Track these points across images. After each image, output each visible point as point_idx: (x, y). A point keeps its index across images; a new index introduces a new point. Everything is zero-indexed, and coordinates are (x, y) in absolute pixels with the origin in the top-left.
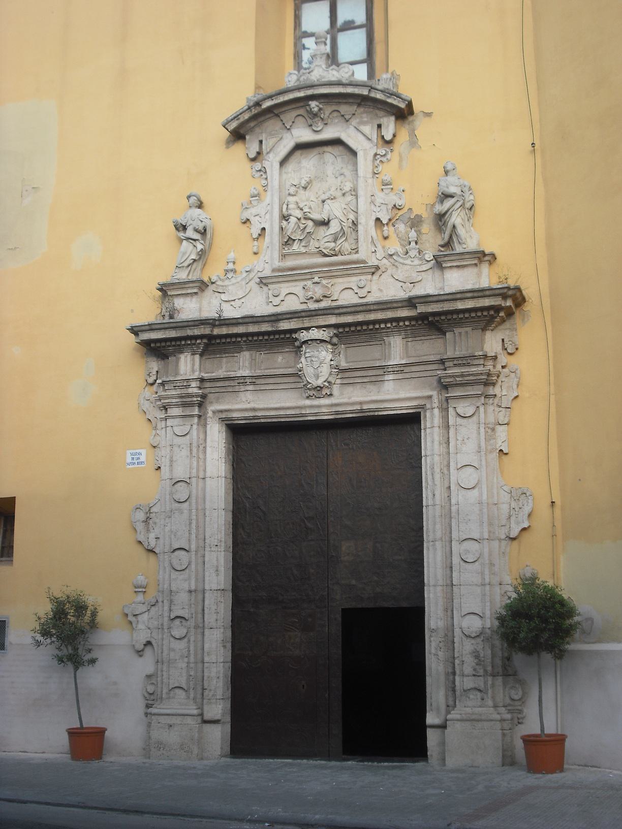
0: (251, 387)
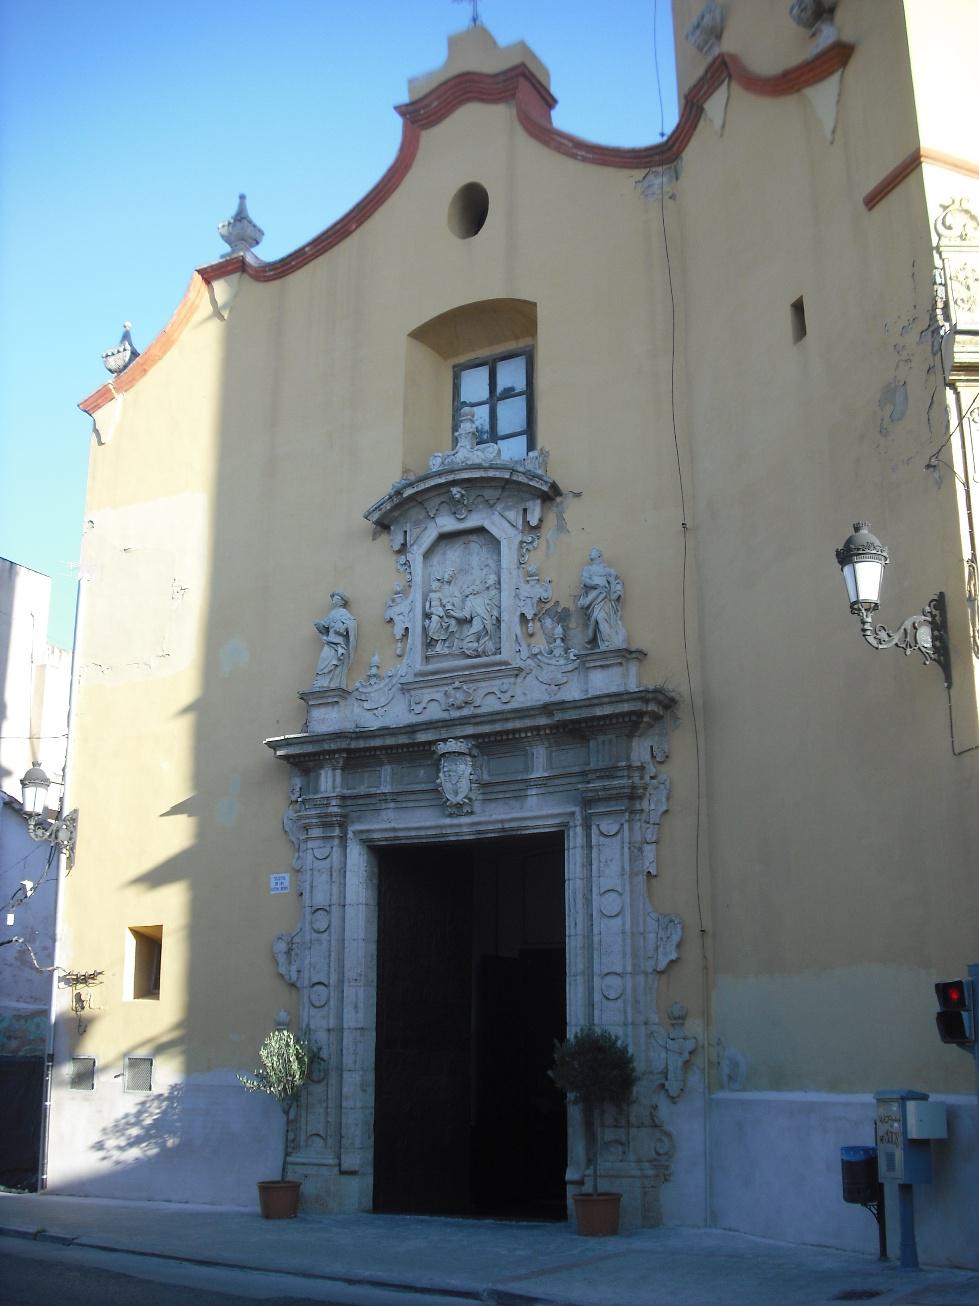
0: (392, 805)
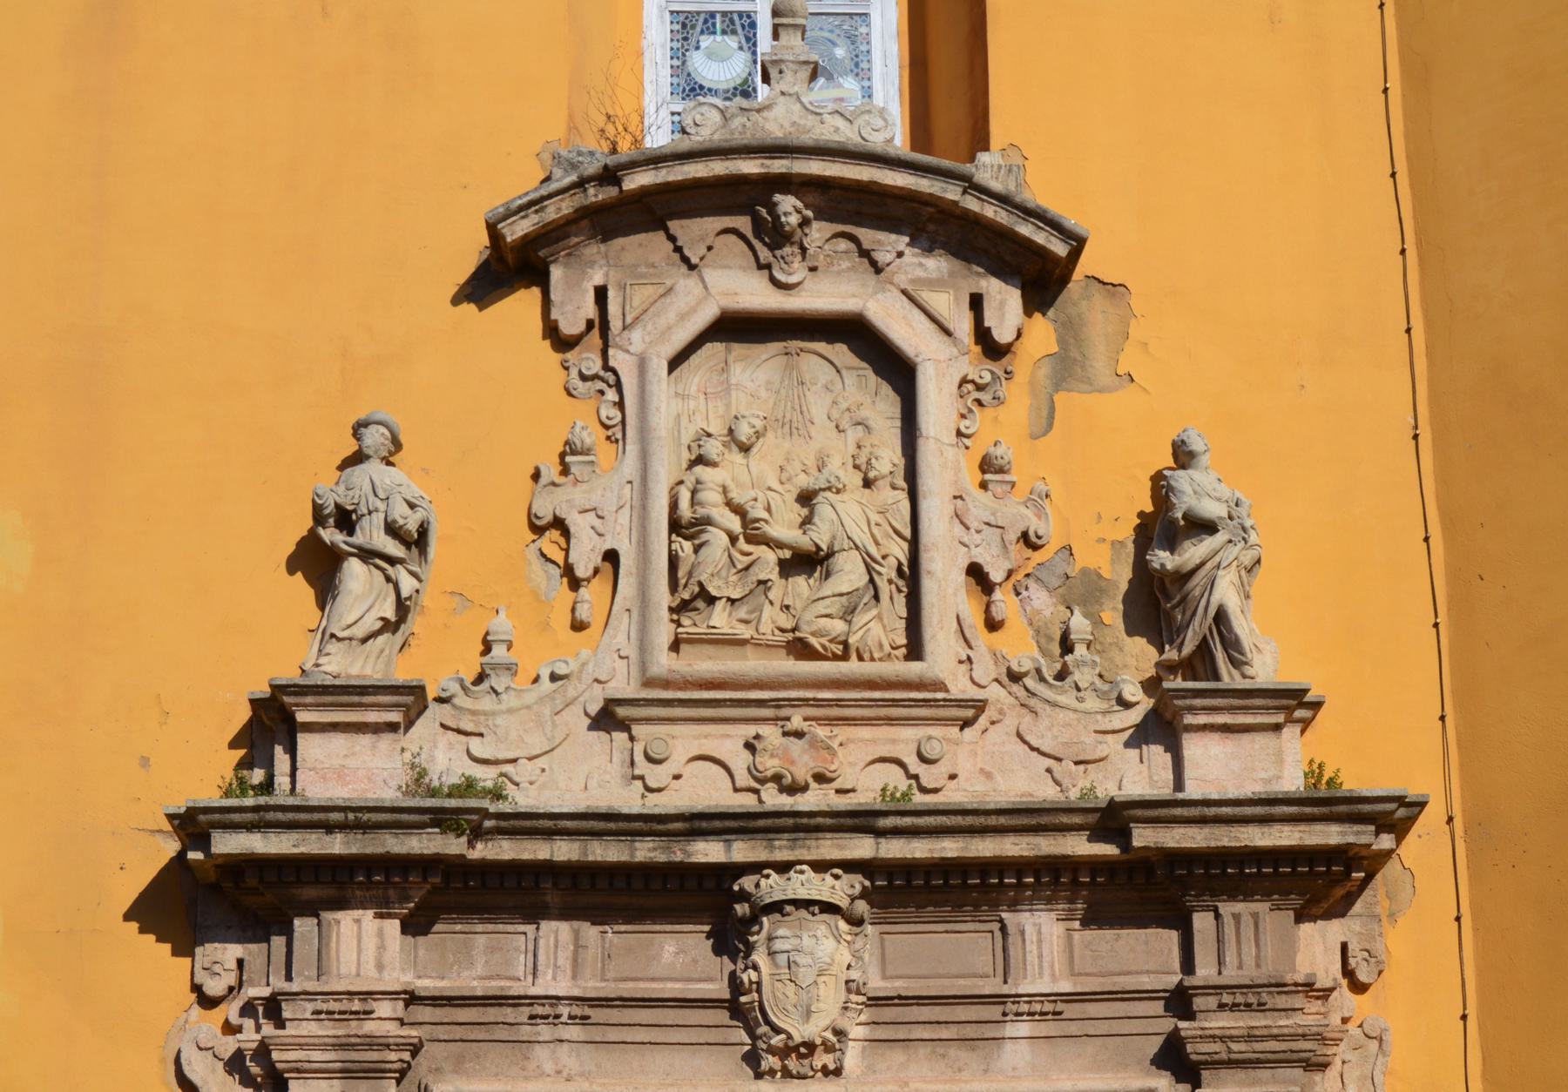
0: (574, 1032)
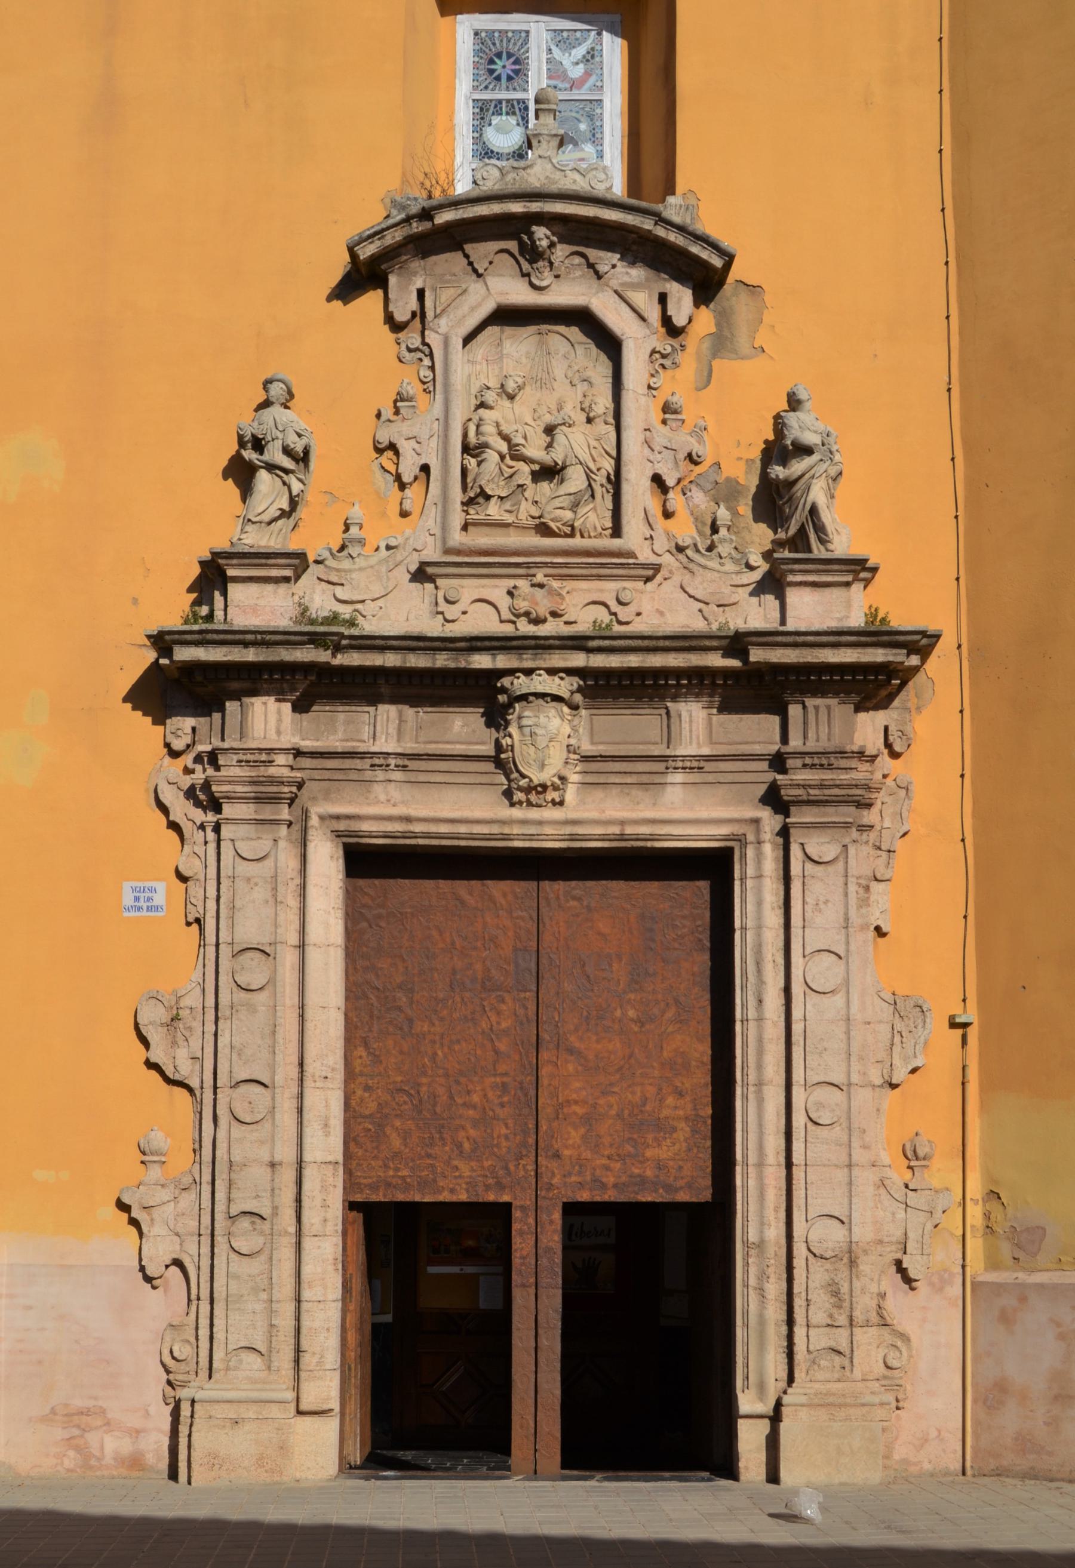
0: (398, 775)
